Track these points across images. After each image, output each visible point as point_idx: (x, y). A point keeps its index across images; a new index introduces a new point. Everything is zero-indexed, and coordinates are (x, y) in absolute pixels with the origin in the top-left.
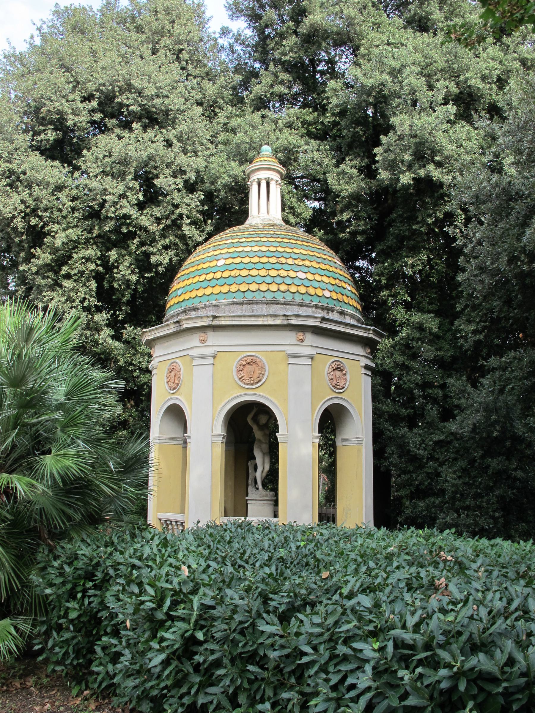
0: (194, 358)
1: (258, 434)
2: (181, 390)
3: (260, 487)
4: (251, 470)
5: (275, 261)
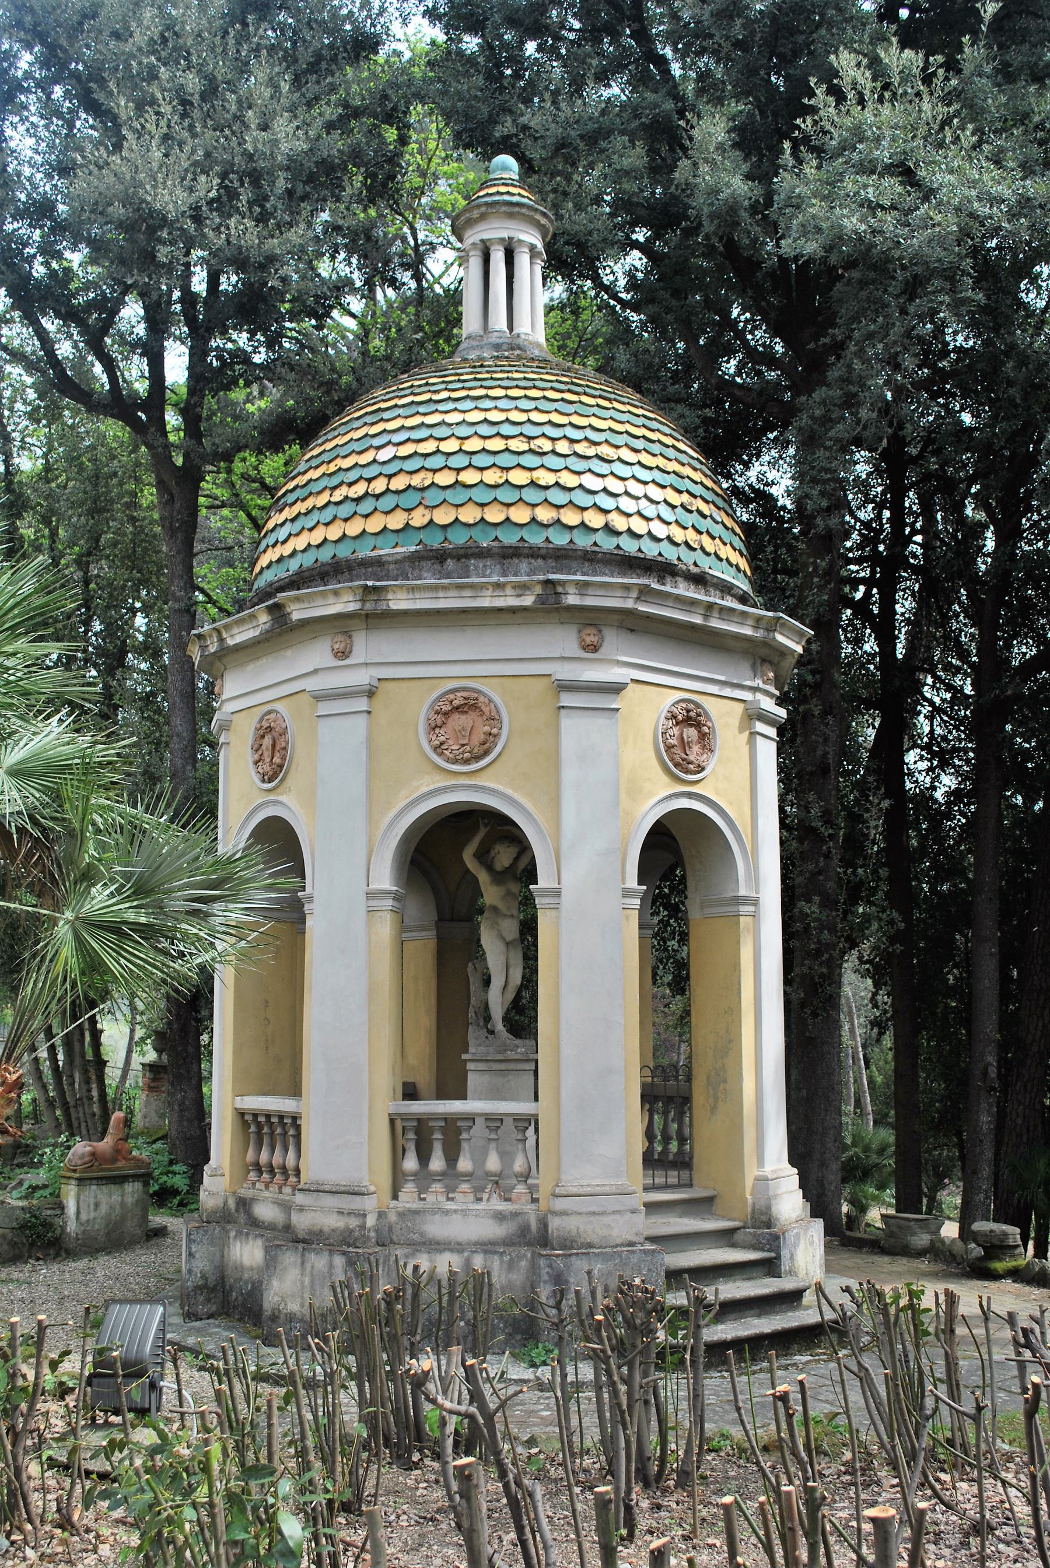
0: (320, 697)
1: (491, 894)
2: (290, 781)
3: (499, 1026)
4: (475, 985)
5: (525, 447)
